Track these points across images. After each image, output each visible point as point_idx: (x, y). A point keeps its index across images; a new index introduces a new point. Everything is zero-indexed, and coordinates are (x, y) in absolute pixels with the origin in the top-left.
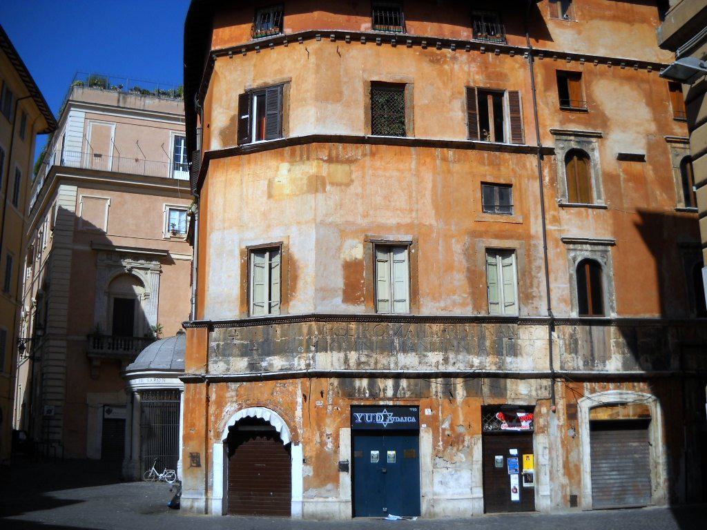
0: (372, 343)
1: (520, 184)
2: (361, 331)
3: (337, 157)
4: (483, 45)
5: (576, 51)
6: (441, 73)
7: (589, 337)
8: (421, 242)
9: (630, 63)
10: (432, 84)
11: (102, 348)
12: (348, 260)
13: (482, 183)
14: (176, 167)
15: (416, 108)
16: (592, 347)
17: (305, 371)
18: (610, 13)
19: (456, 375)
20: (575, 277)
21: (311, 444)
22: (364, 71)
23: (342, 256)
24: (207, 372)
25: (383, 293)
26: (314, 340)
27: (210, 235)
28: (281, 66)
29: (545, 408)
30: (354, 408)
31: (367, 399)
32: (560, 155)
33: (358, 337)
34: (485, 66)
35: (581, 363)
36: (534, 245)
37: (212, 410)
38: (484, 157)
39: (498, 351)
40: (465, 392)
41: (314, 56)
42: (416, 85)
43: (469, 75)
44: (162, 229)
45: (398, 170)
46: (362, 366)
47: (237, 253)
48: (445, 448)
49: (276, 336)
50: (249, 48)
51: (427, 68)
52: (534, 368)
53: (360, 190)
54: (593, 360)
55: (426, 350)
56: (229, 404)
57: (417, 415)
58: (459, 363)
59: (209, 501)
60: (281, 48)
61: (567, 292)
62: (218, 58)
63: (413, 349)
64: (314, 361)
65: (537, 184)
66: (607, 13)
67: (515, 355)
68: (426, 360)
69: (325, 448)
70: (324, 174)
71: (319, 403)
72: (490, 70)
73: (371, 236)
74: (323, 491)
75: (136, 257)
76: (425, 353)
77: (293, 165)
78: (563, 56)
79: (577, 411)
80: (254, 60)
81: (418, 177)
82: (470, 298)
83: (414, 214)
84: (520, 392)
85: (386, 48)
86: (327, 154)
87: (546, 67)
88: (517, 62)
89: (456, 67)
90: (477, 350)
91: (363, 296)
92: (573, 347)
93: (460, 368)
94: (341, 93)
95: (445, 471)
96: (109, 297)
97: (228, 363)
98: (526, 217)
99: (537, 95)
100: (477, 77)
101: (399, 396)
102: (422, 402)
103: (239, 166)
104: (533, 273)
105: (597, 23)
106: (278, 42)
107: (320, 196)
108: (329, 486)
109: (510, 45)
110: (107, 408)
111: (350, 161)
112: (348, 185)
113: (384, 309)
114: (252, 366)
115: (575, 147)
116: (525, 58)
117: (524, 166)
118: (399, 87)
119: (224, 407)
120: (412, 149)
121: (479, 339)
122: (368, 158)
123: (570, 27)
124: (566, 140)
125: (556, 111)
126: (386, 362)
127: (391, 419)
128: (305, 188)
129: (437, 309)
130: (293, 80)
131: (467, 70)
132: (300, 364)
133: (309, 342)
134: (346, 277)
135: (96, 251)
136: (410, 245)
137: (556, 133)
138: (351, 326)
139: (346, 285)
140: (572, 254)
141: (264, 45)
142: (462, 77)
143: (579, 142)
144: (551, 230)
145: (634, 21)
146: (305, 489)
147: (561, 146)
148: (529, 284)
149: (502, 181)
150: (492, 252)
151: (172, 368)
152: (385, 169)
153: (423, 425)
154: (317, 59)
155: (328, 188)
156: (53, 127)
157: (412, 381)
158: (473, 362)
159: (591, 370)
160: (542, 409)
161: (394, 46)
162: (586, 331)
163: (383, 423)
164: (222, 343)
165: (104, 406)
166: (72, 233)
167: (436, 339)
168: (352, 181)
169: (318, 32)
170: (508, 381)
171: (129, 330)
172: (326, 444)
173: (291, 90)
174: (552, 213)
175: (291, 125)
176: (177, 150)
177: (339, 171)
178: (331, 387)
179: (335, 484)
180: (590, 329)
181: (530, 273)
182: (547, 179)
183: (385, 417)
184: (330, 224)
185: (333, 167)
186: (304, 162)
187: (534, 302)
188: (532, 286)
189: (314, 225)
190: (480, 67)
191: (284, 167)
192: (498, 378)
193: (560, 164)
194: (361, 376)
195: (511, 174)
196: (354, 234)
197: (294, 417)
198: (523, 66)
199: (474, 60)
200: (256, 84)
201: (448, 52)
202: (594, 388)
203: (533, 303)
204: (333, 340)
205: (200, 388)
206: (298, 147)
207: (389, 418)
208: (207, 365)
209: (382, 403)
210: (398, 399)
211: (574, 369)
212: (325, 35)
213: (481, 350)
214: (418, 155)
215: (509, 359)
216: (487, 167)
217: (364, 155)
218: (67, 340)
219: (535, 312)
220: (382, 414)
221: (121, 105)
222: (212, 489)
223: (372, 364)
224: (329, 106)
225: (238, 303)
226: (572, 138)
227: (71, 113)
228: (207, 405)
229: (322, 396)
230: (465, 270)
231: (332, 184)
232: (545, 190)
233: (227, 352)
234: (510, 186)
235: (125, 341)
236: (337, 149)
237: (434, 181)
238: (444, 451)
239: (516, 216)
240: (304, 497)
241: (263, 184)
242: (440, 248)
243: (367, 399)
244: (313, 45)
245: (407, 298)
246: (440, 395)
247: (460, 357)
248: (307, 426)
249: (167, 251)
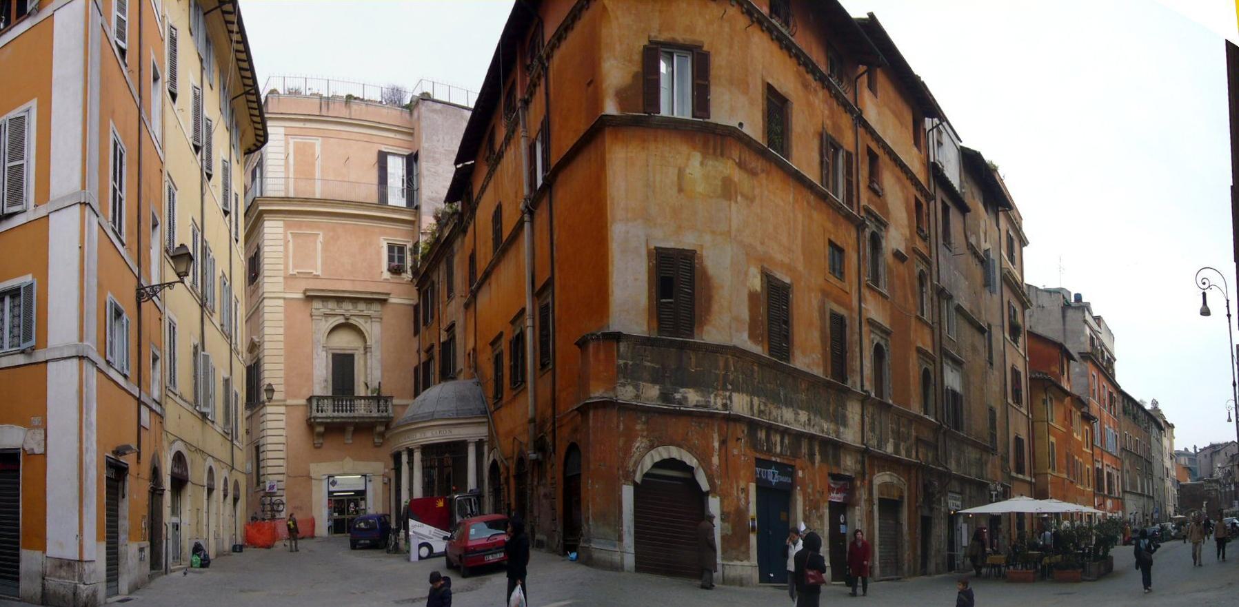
47: (644, 252)
97: (636, 387)
114: (665, 397)
128: (719, 191)
217: (763, 171)
221: (324, 113)
241: (673, 173)
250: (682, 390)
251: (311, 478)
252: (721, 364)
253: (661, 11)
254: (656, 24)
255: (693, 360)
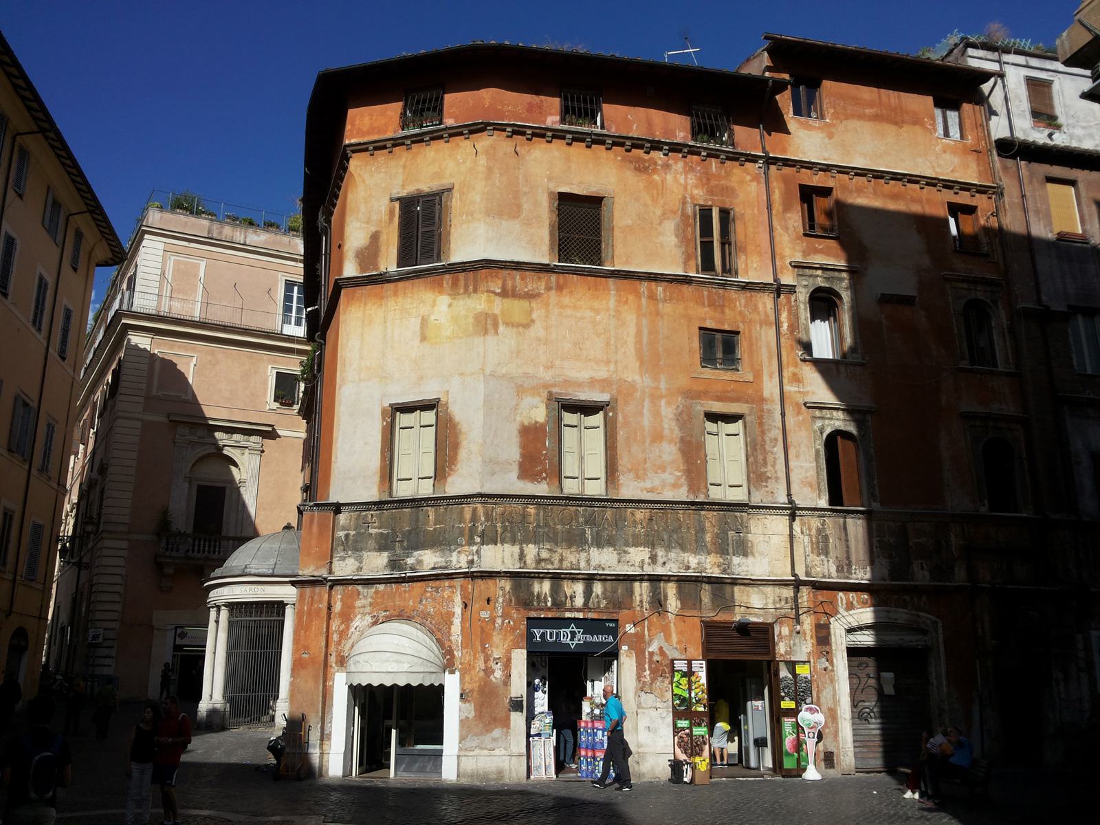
0: (556, 534)
1: (750, 331)
2: (542, 518)
3: (514, 287)
4: (705, 149)
5: (825, 159)
6: (651, 185)
7: (843, 535)
8: (620, 402)
9: (896, 177)
10: (637, 199)
11: (177, 551)
12: (526, 424)
13: (700, 328)
14: (286, 320)
15: (616, 229)
16: (848, 547)
17: (467, 570)
18: (871, 111)
19: (668, 578)
20: (822, 453)
21: (472, 672)
22: (550, 179)
23: (518, 419)
24: (330, 572)
25: (570, 466)
26: (480, 529)
27: (340, 389)
28: (440, 168)
29: (787, 628)
30: (532, 622)
31: (549, 609)
32: (803, 295)
33: (538, 526)
34: (706, 179)
35: (833, 569)
36: (769, 411)
37: (335, 625)
38: (703, 296)
39: (722, 548)
40: (679, 602)
41: (484, 156)
42: (616, 200)
43: (686, 188)
44: (266, 397)
45: (592, 309)
46: (543, 564)
48: (653, 680)
49: (428, 522)
50: (397, 142)
51: (631, 177)
52: (771, 573)
53: (542, 333)
54: (850, 565)
55: (627, 545)
56: (359, 617)
57: (614, 632)
58: (672, 563)
59: (325, 757)
60: (440, 144)
61: (812, 474)
62: (354, 155)
63: (611, 543)
64: (479, 557)
65: (773, 331)
66: (868, 111)
67: (745, 554)
68: (627, 557)
69: (492, 677)
70: (497, 311)
71: (485, 615)
72: (713, 183)
73: (556, 393)
74: (487, 738)
75: (230, 431)
76: (626, 549)
77: (454, 299)
78: (809, 165)
79: (829, 634)
80: (404, 159)
81: (618, 319)
82: (684, 477)
83: (612, 367)
84: (755, 605)
85: (578, 148)
86: (500, 285)
87: (786, 180)
88: (748, 174)
89: (669, 177)
90: (694, 545)
91: (545, 471)
92: (821, 546)
93: (672, 569)
94: (519, 206)
95: (653, 712)
96: (190, 483)
98: (758, 375)
99: (773, 217)
100: (696, 192)
101: (591, 605)
102: (623, 615)
103: (382, 298)
104: (767, 447)
105: (854, 124)
106: (436, 136)
107: (491, 339)
108: (497, 733)
109: (739, 150)
110: (179, 631)
111: (530, 296)
112: (527, 326)
113: (571, 488)
114: (394, 564)
115: (823, 285)
116: (759, 167)
117: (756, 309)
118: (596, 202)
119: (352, 620)
120: (611, 281)
121: (697, 532)
122: (553, 293)
123: (819, 128)
124: (811, 276)
125: (798, 238)
126: (573, 559)
127: (581, 638)
129: (642, 491)
130: (456, 187)
131: (681, 181)
132: (459, 560)
133: (472, 532)
134: (524, 447)
135: (175, 424)
136: (607, 405)
137: (797, 266)
138: (528, 510)
139: (523, 456)
140: (819, 423)
141: (418, 139)
142: (676, 191)
143: (827, 279)
144: (790, 392)
145: (903, 122)
146: (462, 739)
147: (805, 283)
148: (761, 461)
149: (727, 327)
150: (713, 417)
151: (276, 573)
152: (575, 308)
153: (623, 647)
154: (488, 159)
155: (501, 328)
156: (120, 257)
157: (608, 584)
158: (688, 562)
159: (848, 578)
160: (783, 629)
161: (589, 147)
162: (840, 526)
163: (570, 643)
164: (352, 533)
165: (176, 628)
166: (142, 398)
167: (640, 530)
168: (533, 321)
169: (490, 124)
170: (736, 589)
171: (217, 521)
172: (493, 672)
173: (454, 200)
174: (791, 369)
175: (453, 246)
176: (288, 299)
177: (516, 307)
178: (501, 593)
179: (505, 730)
180: (845, 523)
181: (763, 446)
182: (785, 326)
183: (573, 634)
184: (504, 376)
185: (509, 303)
186: (470, 294)
187: (768, 484)
188: (765, 464)
189: (482, 378)
190: (700, 179)
191: (444, 300)
192: (722, 585)
193: (802, 306)
194: (540, 577)
195: (739, 318)
196: (534, 391)
197: (449, 634)
198: (756, 178)
199: (692, 169)
200: (405, 191)
201: (658, 156)
202: (852, 603)
203: (767, 486)
204: (505, 529)
205: (320, 595)
206: (462, 276)
207: (579, 636)
208: (331, 563)
209: (568, 615)
210: (590, 610)
211: (824, 577)
212: (500, 128)
213: (699, 547)
214: (618, 290)
215: (736, 560)
216: (706, 309)
217: (549, 288)
218: (128, 540)
219: (770, 499)
220: (568, 631)
222: (329, 739)
223: (556, 562)
224: (503, 222)
225: (377, 479)
226: (819, 272)
227: (144, 243)
228: (329, 618)
229: (488, 603)
230: (678, 440)
231: (507, 324)
232: (783, 340)
233: (359, 545)
234: (738, 333)
235: (210, 541)
236: (514, 278)
237: (639, 326)
238: (651, 684)
239: (744, 373)
240: (460, 749)
241: (415, 324)
242: (645, 411)
243: (549, 609)
244: (484, 141)
245: (603, 476)
246: (646, 605)
247: (672, 555)
248: (467, 647)
249: (272, 426)
250: (416, 553)
251: (152, 628)
252: (468, 516)
253: (404, 167)
254: (399, 180)
255: (432, 517)
